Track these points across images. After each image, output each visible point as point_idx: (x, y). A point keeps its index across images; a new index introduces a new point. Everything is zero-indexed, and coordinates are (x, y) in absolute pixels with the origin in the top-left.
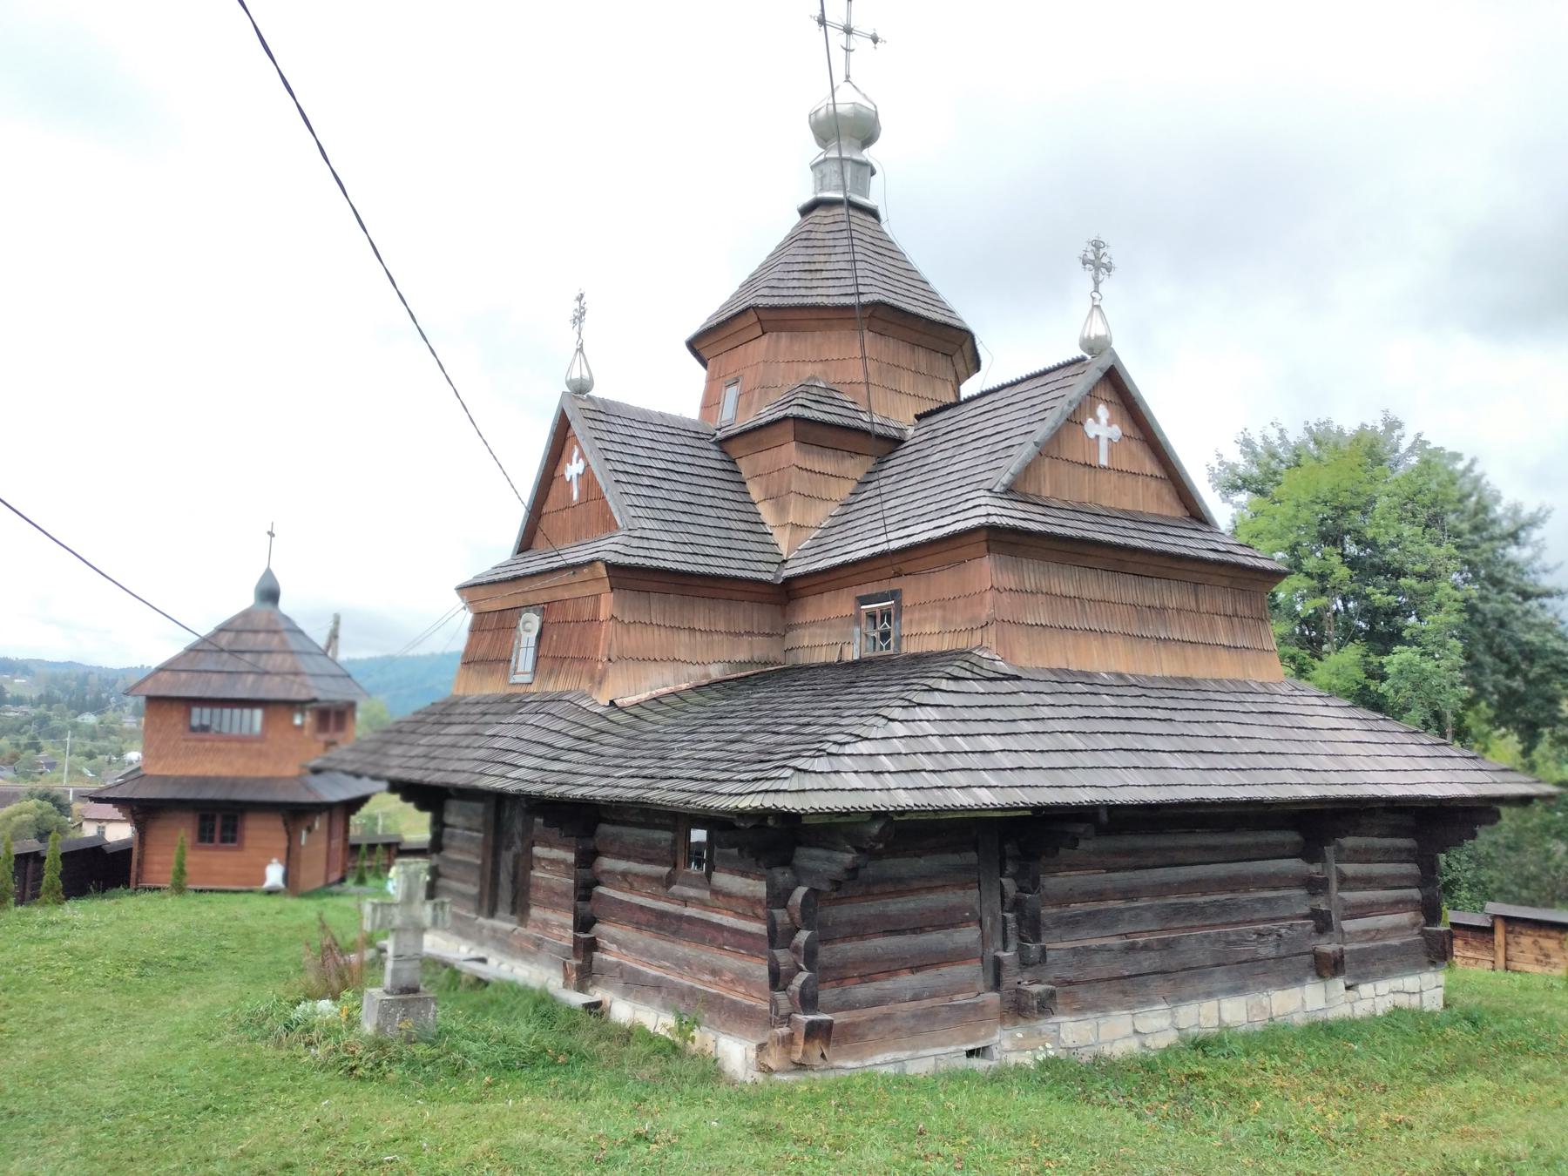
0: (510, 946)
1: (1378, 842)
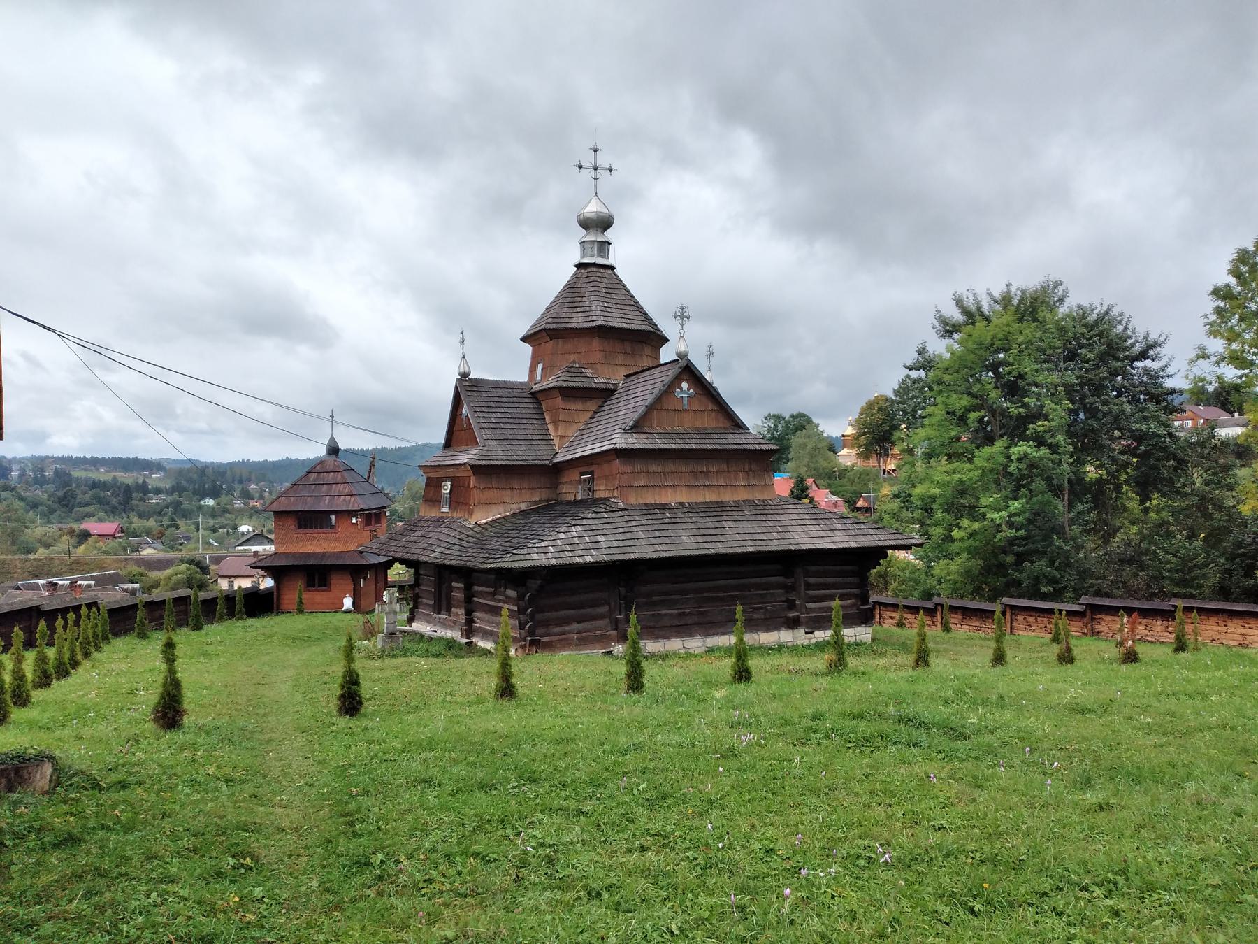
0: (445, 625)
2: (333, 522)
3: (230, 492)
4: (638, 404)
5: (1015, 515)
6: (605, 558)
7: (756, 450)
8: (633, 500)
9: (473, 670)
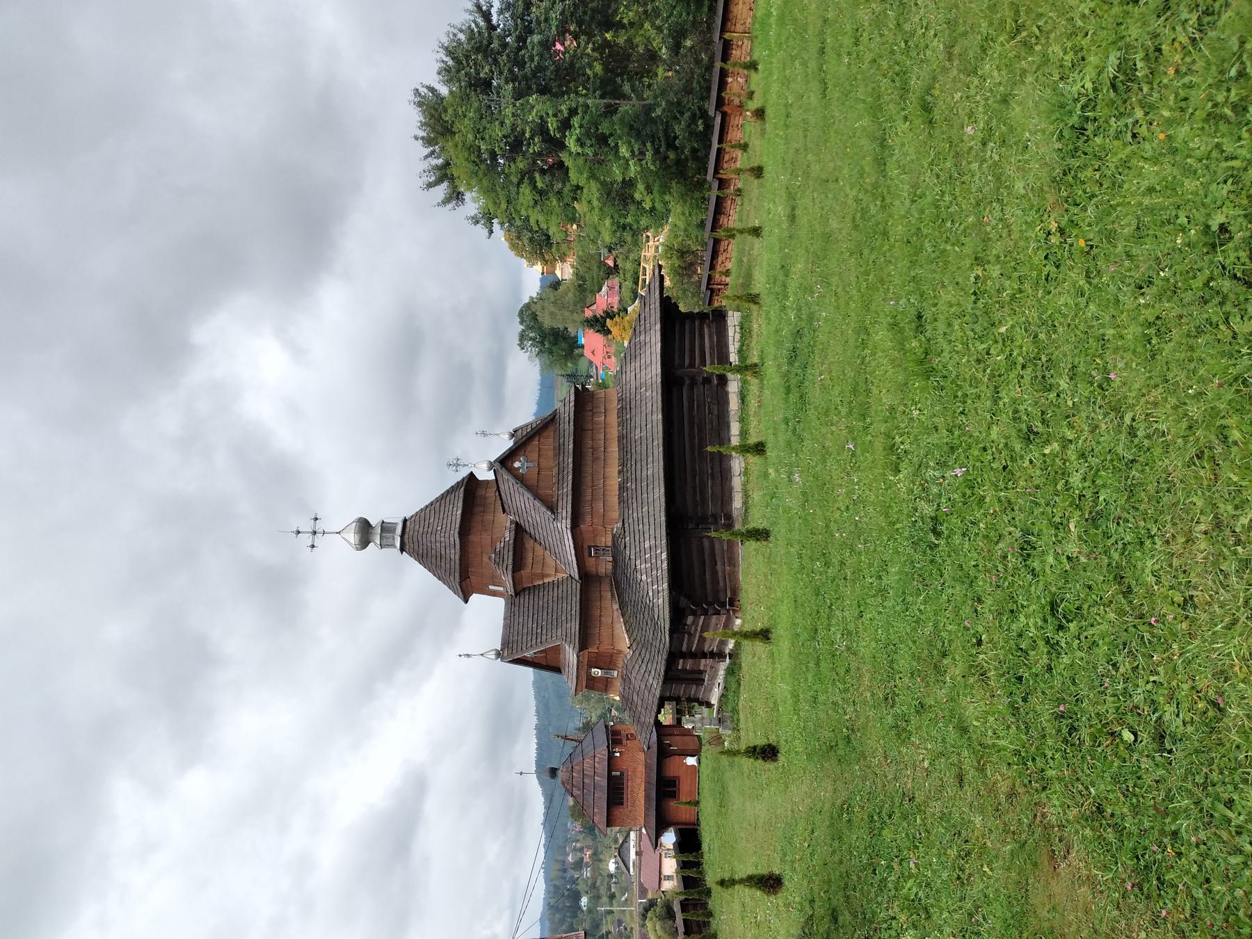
1: (677, 344)
2: (618, 773)
3: (574, 881)
4: (531, 505)
5: (632, 152)
6: (664, 542)
7: (575, 406)
8: (615, 513)
9: (751, 656)
